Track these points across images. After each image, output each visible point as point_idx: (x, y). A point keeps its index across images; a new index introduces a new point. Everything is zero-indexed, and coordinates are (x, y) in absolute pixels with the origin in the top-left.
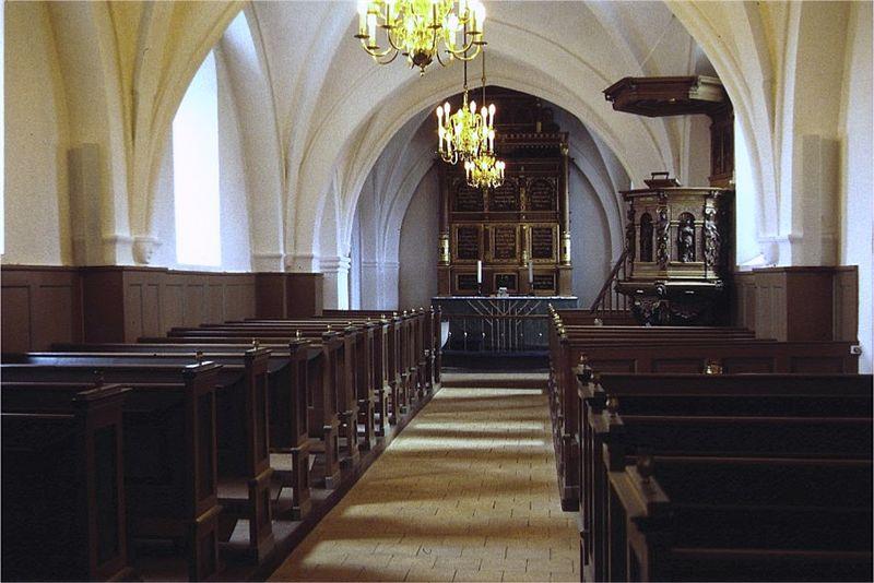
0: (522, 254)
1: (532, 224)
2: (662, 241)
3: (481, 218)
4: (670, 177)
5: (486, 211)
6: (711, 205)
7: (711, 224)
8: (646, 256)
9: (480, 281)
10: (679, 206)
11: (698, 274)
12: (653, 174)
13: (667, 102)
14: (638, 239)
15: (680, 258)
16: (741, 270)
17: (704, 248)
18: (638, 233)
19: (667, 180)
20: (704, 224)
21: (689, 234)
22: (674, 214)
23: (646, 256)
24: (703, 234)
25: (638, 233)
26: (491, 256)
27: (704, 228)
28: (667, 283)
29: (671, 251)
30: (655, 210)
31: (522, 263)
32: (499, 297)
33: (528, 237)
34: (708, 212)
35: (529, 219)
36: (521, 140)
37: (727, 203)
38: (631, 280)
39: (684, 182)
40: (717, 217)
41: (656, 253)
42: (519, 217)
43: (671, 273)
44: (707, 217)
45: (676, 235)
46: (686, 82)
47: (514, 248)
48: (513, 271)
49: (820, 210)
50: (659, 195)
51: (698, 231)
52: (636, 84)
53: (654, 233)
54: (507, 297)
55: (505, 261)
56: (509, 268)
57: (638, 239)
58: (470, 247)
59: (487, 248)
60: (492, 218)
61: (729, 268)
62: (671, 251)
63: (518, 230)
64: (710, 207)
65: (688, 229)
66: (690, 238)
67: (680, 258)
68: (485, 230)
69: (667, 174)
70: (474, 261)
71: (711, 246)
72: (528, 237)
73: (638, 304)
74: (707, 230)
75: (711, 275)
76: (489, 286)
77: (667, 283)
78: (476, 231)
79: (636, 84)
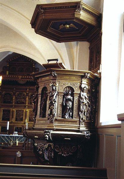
0: (25, 120)
1: (30, 109)
2: (52, 104)
3: (12, 106)
4: (59, 62)
5: (14, 104)
6: (85, 83)
7: (84, 94)
8: (43, 115)
9: (8, 129)
10: (64, 82)
11: (74, 126)
12: (49, 60)
13: (65, 28)
14: (39, 104)
15: (63, 116)
16: (103, 125)
17: (79, 110)
18: (40, 100)
19: (57, 64)
20: (80, 94)
21: (70, 100)
22: (60, 86)
23: (43, 115)
24: (79, 101)
25: (40, 100)
26: (14, 120)
27: (80, 97)
28: (52, 132)
29: (57, 110)
30: (49, 85)
31: (25, 123)
32: (14, 135)
33: (28, 114)
34: (83, 86)
35: (29, 107)
36: (28, 79)
37: (95, 84)
38: (34, 129)
39: (67, 67)
40: (89, 91)
41: (48, 112)
42: (25, 106)
43: (56, 125)
44: (82, 89)
45: (61, 101)
46: (72, 7)
47: (23, 117)
48: (22, 126)
49: (109, 127)
50: (51, 74)
51: (76, 98)
52: (43, 9)
53: (48, 99)
54: (17, 135)
55: (19, 122)
56: (19, 124)
57: (39, 104)
58: (7, 116)
59: (13, 117)
60: (15, 107)
61: (96, 124)
62: (57, 110)
63: (25, 111)
64: (85, 83)
65: (69, 97)
66: (70, 103)
67: (63, 116)
68: (13, 111)
69: (57, 60)
70: (5, 122)
71: (83, 108)
72: (28, 114)
73: (36, 145)
74: (82, 98)
75: (83, 128)
76: (11, 131)
77: (52, 132)
78: (9, 111)
79: (43, 9)
